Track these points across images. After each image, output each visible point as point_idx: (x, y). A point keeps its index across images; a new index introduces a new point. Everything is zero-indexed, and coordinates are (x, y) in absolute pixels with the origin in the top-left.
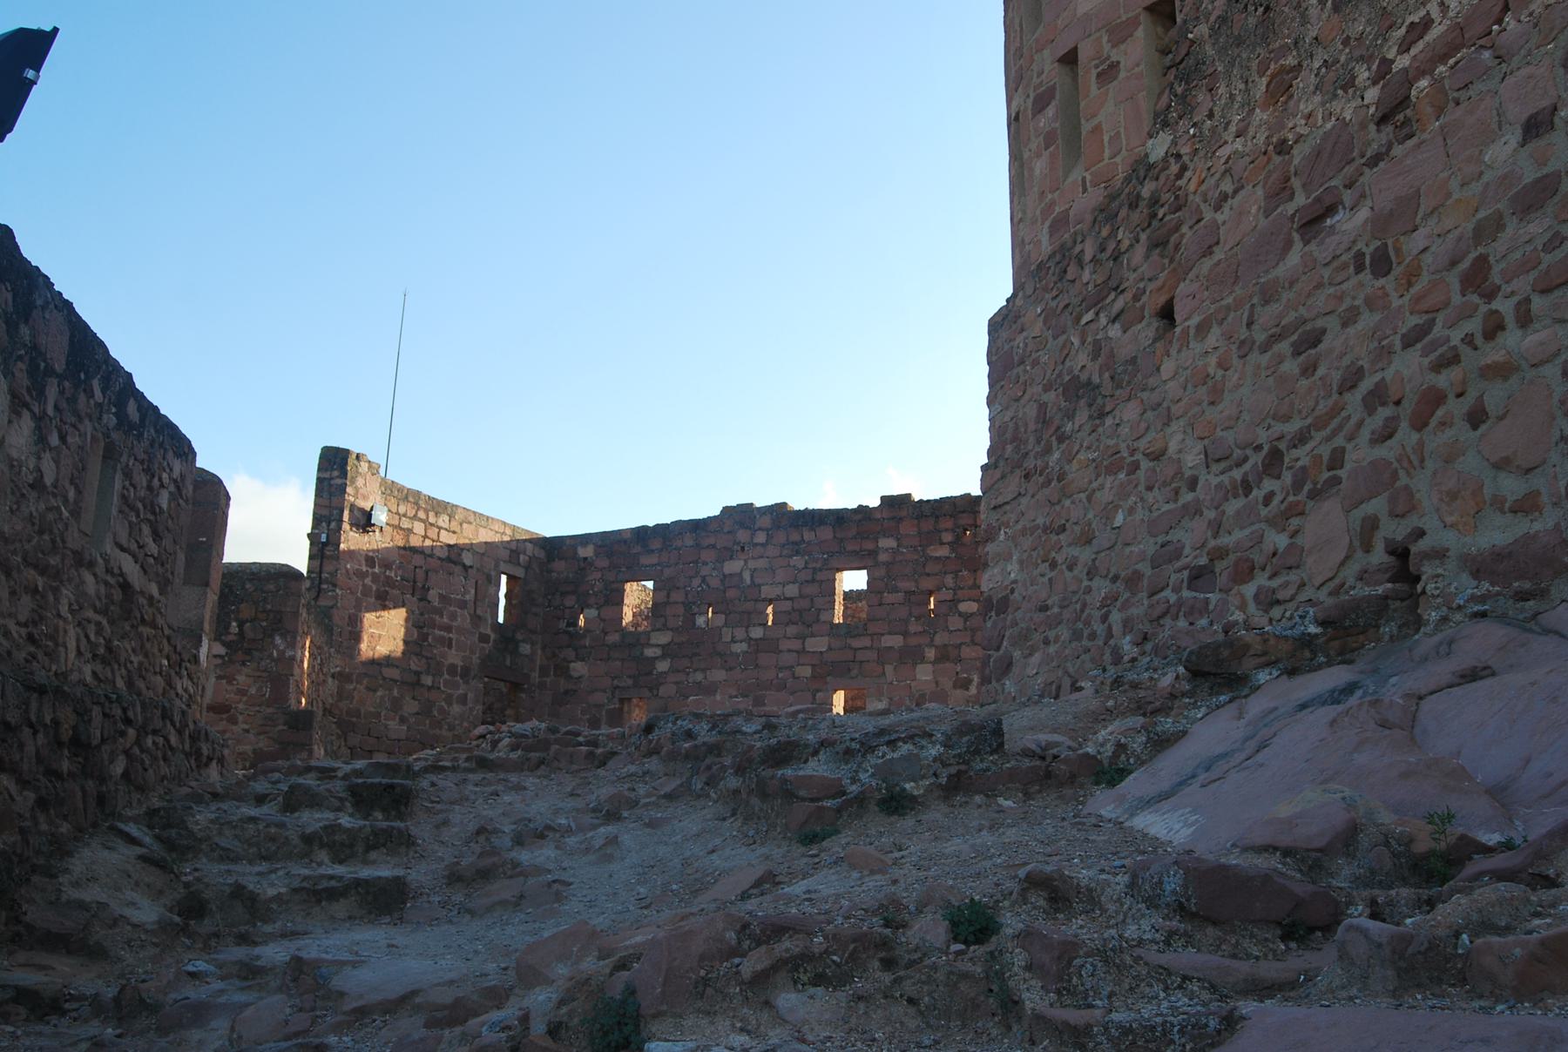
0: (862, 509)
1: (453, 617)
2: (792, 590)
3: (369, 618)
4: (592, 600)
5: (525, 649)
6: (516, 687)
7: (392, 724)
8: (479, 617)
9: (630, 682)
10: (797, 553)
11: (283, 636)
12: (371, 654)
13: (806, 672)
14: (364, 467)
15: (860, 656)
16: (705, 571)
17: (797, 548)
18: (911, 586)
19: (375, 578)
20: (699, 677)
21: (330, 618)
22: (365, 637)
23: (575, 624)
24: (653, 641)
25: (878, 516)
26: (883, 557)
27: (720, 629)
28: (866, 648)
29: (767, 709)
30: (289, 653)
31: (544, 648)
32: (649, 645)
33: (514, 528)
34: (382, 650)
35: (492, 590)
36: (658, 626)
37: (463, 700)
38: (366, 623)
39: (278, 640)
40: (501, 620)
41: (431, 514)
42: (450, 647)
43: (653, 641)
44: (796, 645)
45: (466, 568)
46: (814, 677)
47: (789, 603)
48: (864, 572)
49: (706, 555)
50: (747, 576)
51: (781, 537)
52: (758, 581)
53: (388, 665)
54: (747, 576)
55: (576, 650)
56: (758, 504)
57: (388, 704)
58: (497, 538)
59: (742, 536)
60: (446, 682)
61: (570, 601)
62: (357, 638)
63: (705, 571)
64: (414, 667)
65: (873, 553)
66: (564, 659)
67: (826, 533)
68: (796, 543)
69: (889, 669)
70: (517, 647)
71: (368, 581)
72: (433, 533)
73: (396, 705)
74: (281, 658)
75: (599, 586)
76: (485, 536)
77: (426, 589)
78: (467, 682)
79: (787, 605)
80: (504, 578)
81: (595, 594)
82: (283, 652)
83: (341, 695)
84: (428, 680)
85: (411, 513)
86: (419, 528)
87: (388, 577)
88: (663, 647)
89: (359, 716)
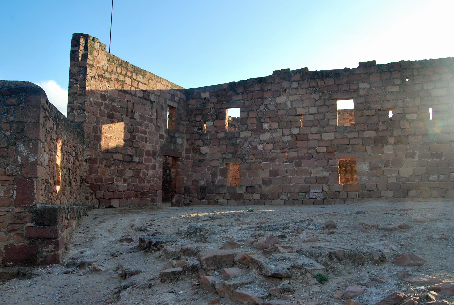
0: (346, 70)
1: (147, 127)
2: (313, 110)
3: (105, 127)
4: (209, 118)
5: (179, 141)
6: (175, 159)
7: (120, 183)
8: (159, 127)
9: (231, 156)
10: (315, 92)
11: (26, 143)
12: (106, 147)
13: (324, 150)
14: (97, 45)
15: (352, 142)
16: (266, 102)
17: (315, 89)
19: (107, 106)
21: (82, 128)
22: (103, 139)
23: (202, 129)
25: (358, 72)
28: (355, 138)
29: (303, 168)
30: (32, 158)
31: (187, 140)
32: (239, 138)
33: (172, 84)
34: (112, 144)
35: (164, 113)
36: (244, 129)
37: (154, 168)
38: (103, 131)
39: (21, 147)
41: (134, 74)
42: (146, 142)
44: (317, 137)
45: (152, 102)
46: (327, 152)
47: (312, 116)
49: (266, 95)
50: (289, 104)
52: (294, 106)
53: (116, 153)
54: (289, 104)
55: (203, 141)
57: (117, 173)
58: (165, 88)
59: (285, 84)
61: (199, 118)
62: (99, 139)
63: (266, 102)
64: (129, 153)
65: (357, 91)
67: (330, 82)
68: (314, 87)
69: (369, 148)
70: (176, 141)
71: (103, 108)
72: (135, 84)
73: (121, 173)
75: (213, 111)
76: (159, 87)
78: (155, 159)
79: (311, 118)
83: (91, 171)
84: (136, 159)
85: (124, 73)
86: (128, 81)
87: (113, 106)
89: (102, 181)
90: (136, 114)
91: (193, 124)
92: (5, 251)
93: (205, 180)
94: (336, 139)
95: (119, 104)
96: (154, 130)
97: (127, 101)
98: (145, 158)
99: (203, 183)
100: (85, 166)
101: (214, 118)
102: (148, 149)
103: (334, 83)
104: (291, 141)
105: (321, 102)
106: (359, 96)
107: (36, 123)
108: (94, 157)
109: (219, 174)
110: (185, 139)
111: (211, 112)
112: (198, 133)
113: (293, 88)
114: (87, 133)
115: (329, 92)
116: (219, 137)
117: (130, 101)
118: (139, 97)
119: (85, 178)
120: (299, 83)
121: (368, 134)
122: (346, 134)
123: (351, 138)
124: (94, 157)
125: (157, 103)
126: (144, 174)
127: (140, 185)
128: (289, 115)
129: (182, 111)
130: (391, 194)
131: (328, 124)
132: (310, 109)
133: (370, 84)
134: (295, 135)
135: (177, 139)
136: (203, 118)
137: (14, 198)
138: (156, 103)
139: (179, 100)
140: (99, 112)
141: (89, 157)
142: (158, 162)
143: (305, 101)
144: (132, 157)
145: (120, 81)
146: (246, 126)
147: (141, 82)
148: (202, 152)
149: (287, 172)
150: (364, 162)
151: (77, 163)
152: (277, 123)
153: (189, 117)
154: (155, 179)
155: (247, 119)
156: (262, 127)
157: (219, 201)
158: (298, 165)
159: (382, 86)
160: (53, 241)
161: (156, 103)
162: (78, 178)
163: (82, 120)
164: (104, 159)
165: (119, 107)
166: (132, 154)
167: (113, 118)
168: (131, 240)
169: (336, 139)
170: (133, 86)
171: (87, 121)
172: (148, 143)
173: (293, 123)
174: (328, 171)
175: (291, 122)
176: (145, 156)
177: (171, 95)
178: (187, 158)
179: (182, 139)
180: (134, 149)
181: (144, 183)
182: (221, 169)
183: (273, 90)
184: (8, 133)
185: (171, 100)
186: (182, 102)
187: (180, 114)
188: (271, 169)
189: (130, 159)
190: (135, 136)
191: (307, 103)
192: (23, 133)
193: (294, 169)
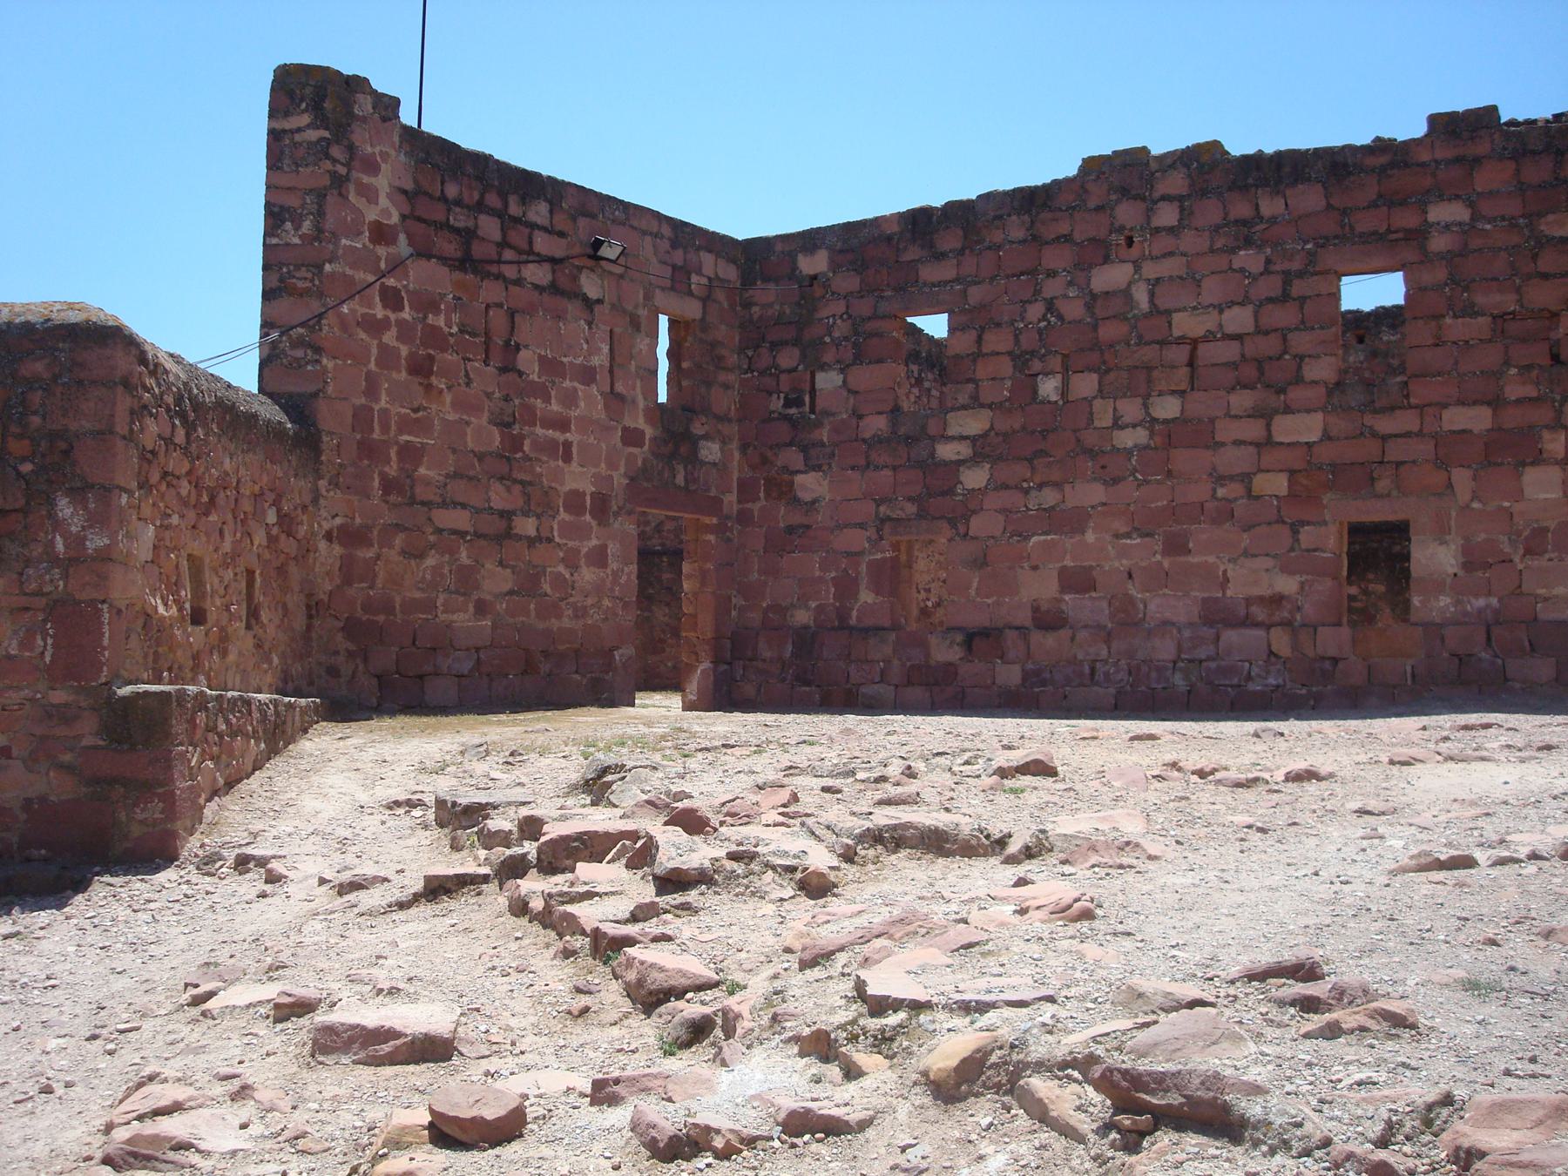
0: (1382, 146)
1: (570, 399)
2: (1239, 319)
5: (711, 451)
8: (621, 398)
9: (911, 509)
10: (1248, 242)
11: (78, 493)
13: (1278, 484)
15: (1395, 452)
16: (1052, 288)
17: (1246, 233)
18: (1509, 302)
20: (1049, 497)
24: (952, 431)
25: (1425, 157)
26: (1439, 243)
27: (1089, 402)
28: (1407, 435)
30: (96, 542)
31: (744, 447)
35: (642, 344)
36: (963, 399)
37: (599, 558)
40: (662, 397)
41: (513, 202)
42: (568, 458)
43: (952, 431)
44: (1254, 430)
45: (589, 304)
46: (1293, 496)
48: (1399, 275)
50: (1141, 295)
51: (1210, 212)
52: (1163, 303)
54: (1141, 295)
55: (804, 449)
56: (1156, 150)
59: (1128, 213)
60: (564, 526)
63: (1052, 288)
64: (497, 503)
65: (1418, 235)
66: (785, 469)
67: (1309, 198)
68: (1244, 222)
69: (1462, 478)
70: (694, 451)
71: (389, 337)
73: (466, 580)
74: (75, 560)
75: (842, 328)
77: (512, 349)
80: (663, 321)
81: (837, 344)
82: (81, 540)
83: (348, 572)
84: (527, 526)
88: (973, 440)
90: (523, 354)
91: (769, 382)
92: (24, 817)
93: (813, 604)
94: (1330, 438)
95: (455, 318)
96: (599, 412)
97: (488, 306)
98: (562, 525)
99: (802, 617)
100: (328, 554)
101: (849, 355)
102: (574, 486)
103: (1324, 203)
104: (1146, 447)
105: (1269, 287)
106: (1426, 258)
107: (104, 434)
108: (358, 521)
109: (864, 581)
110: (734, 445)
111: (837, 334)
112: (787, 418)
113: (1157, 230)
114: (331, 433)
115: (1306, 242)
116: (867, 435)
117: (500, 305)
118: (536, 287)
119: (325, 598)
120: (1182, 209)
121: (1458, 418)
122: (1369, 420)
123: (1391, 436)
124: (358, 521)
125: (613, 306)
126: (559, 581)
127: (541, 626)
128: (1141, 341)
129: (721, 332)
130: (1543, 669)
131: (1298, 380)
132: (1227, 314)
133: (1471, 205)
134: (1166, 421)
135: (702, 443)
136: (804, 356)
137: (48, 659)
138: (607, 306)
139: (710, 287)
140: (374, 351)
141: (338, 521)
142: (619, 539)
143: (1206, 284)
144: (510, 520)
145: (457, 231)
146: (971, 386)
147: (545, 229)
148: (800, 494)
149: (1130, 576)
150: (1441, 533)
151: (288, 545)
152: (1095, 376)
153: (750, 353)
154: (606, 602)
155: (974, 361)
156: (1035, 392)
157: (863, 690)
158: (1177, 546)
159: (1523, 216)
160: (160, 791)
161: (607, 306)
162: (295, 600)
163: (312, 388)
164: (398, 527)
165: (455, 330)
166: (508, 507)
167: (430, 373)
168: (420, 804)
169: (1330, 438)
170: (510, 247)
171: (330, 389)
172: (574, 464)
173: (1155, 373)
174: (1292, 573)
175: (1149, 369)
176: (563, 515)
177: (674, 267)
178: (744, 518)
179: (723, 442)
180: (517, 489)
181: (559, 617)
182: (871, 564)
183: (1078, 237)
184: (27, 468)
185: (672, 289)
186: (720, 295)
187: (713, 345)
188: (1069, 563)
189: (503, 524)
190: (522, 437)
191: (1212, 290)
192: (61, 466)
193: (1159, 563)
